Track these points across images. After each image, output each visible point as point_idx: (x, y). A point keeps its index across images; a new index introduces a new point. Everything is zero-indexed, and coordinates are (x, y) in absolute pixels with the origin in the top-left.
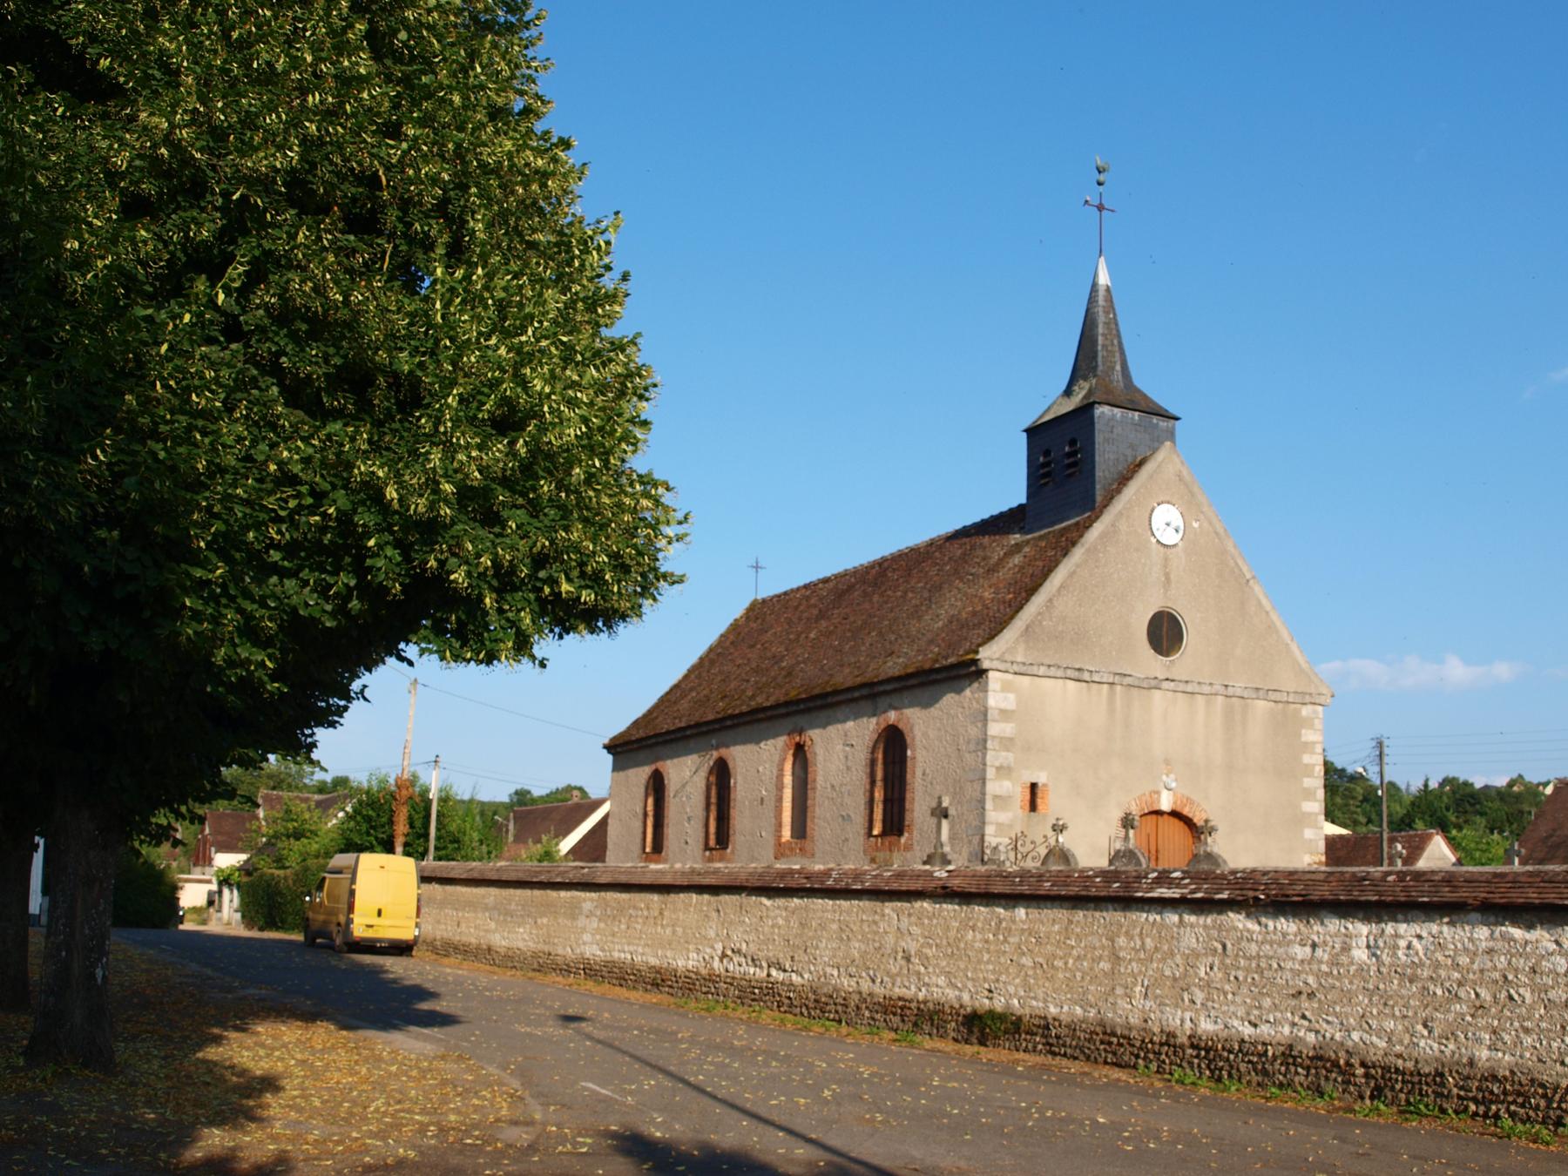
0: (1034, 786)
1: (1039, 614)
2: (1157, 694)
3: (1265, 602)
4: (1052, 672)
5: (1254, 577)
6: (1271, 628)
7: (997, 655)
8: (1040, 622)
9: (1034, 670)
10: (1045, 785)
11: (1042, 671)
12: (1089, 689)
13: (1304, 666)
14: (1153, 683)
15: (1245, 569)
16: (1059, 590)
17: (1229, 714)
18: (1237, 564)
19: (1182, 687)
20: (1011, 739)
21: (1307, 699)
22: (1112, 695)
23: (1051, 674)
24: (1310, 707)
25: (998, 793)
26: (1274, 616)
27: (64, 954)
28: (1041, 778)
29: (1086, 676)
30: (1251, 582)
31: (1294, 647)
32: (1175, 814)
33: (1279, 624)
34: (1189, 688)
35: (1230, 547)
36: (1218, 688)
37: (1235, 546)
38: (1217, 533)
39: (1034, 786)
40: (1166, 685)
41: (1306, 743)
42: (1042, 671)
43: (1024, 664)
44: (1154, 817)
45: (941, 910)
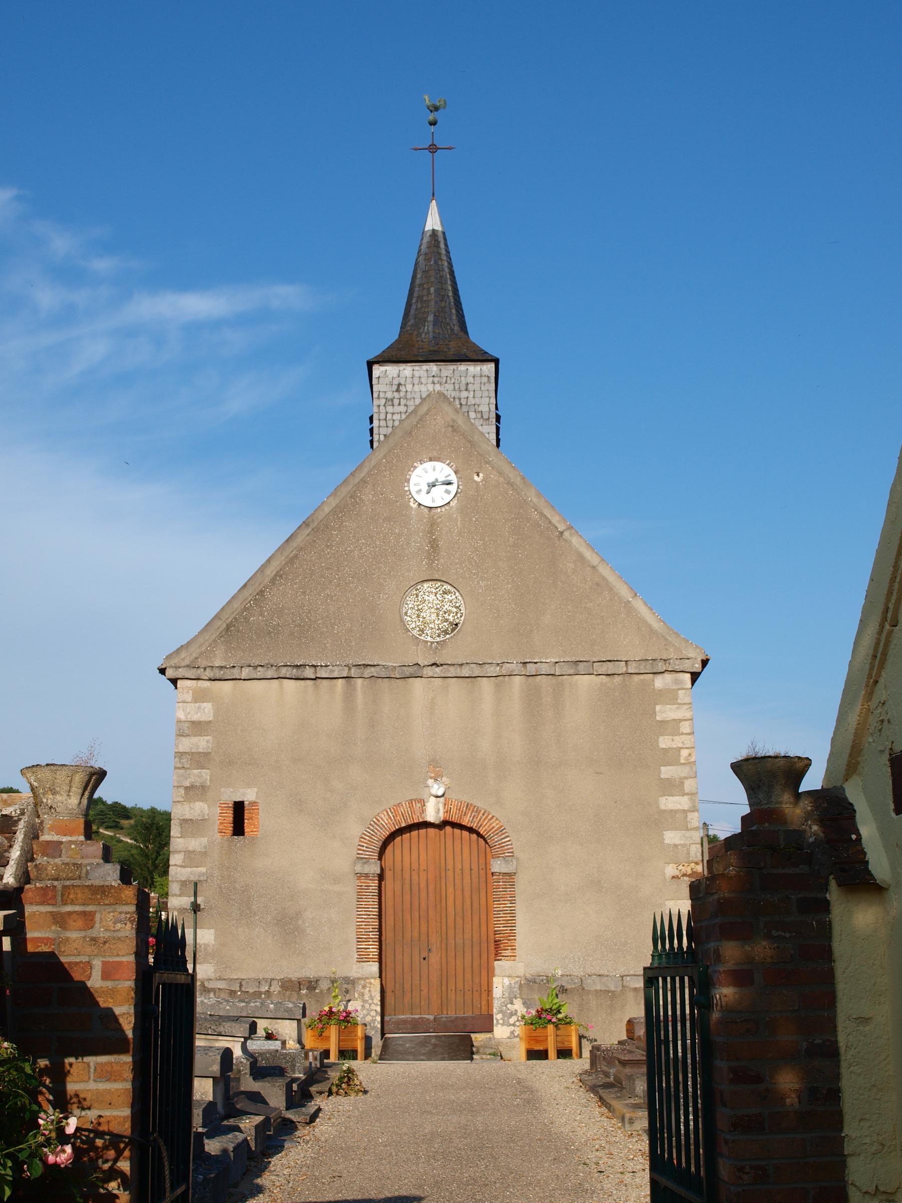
0: (239, 808)
1: (245, 609)
2: (417, 684)
3: (588, 554)
4: (260, 672)
5: (570, 528)
6: (602, 585)
7: (187, 662)
8: (246, 619)
9: (236, 673)
10: (253, 803)
11: (245, 673)
12: (316, 687)
13: (656, 625)
14: (408, 671)
15: (555, 520)
16: (273, 581)
17: (532, 700)
18: (541, 514)
19: (452, 671)
20: (206, 754)
21: (661, 667)
22: (349, 696)
23: (259, 675)
24: (668, 677)
25: (187, 817)
26: (604, 571)
27: (147, 1025)
28: (248, 796)
29: (309, 673)
30: (567, 534)
31: (639, 605)
32: (445, 823)
33: (612, 579)
34: (465, 672)
35: (532, 497)
36: (514, 667)
37: (539, 495)
38: (511, 484)
39: (239, 808)
40: (428, 671)
41: (663, 722)
42: (245, 673)
43: (221, 668)
44: (488, 410)
45: (300, 1009)
